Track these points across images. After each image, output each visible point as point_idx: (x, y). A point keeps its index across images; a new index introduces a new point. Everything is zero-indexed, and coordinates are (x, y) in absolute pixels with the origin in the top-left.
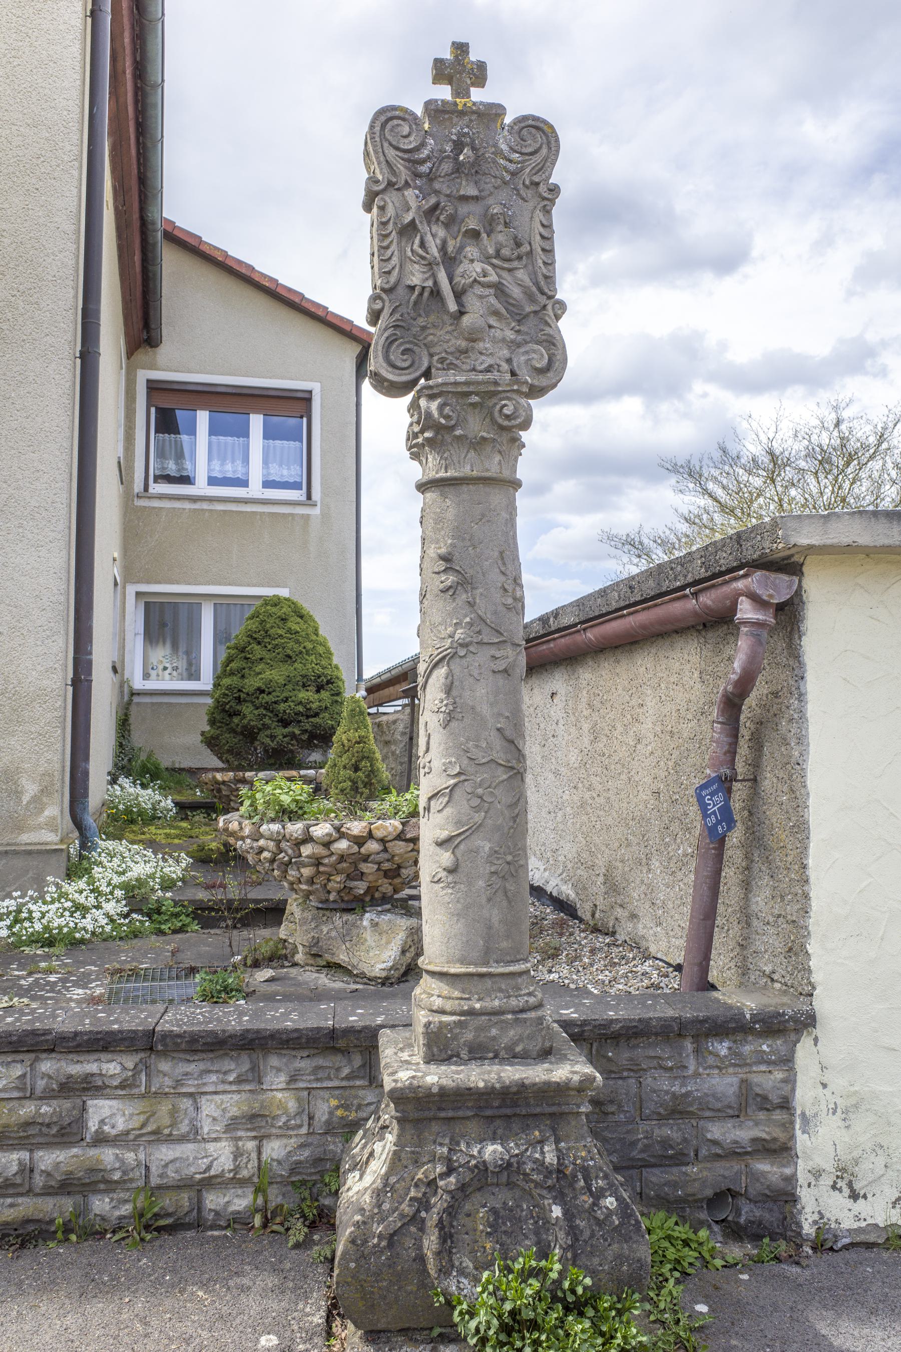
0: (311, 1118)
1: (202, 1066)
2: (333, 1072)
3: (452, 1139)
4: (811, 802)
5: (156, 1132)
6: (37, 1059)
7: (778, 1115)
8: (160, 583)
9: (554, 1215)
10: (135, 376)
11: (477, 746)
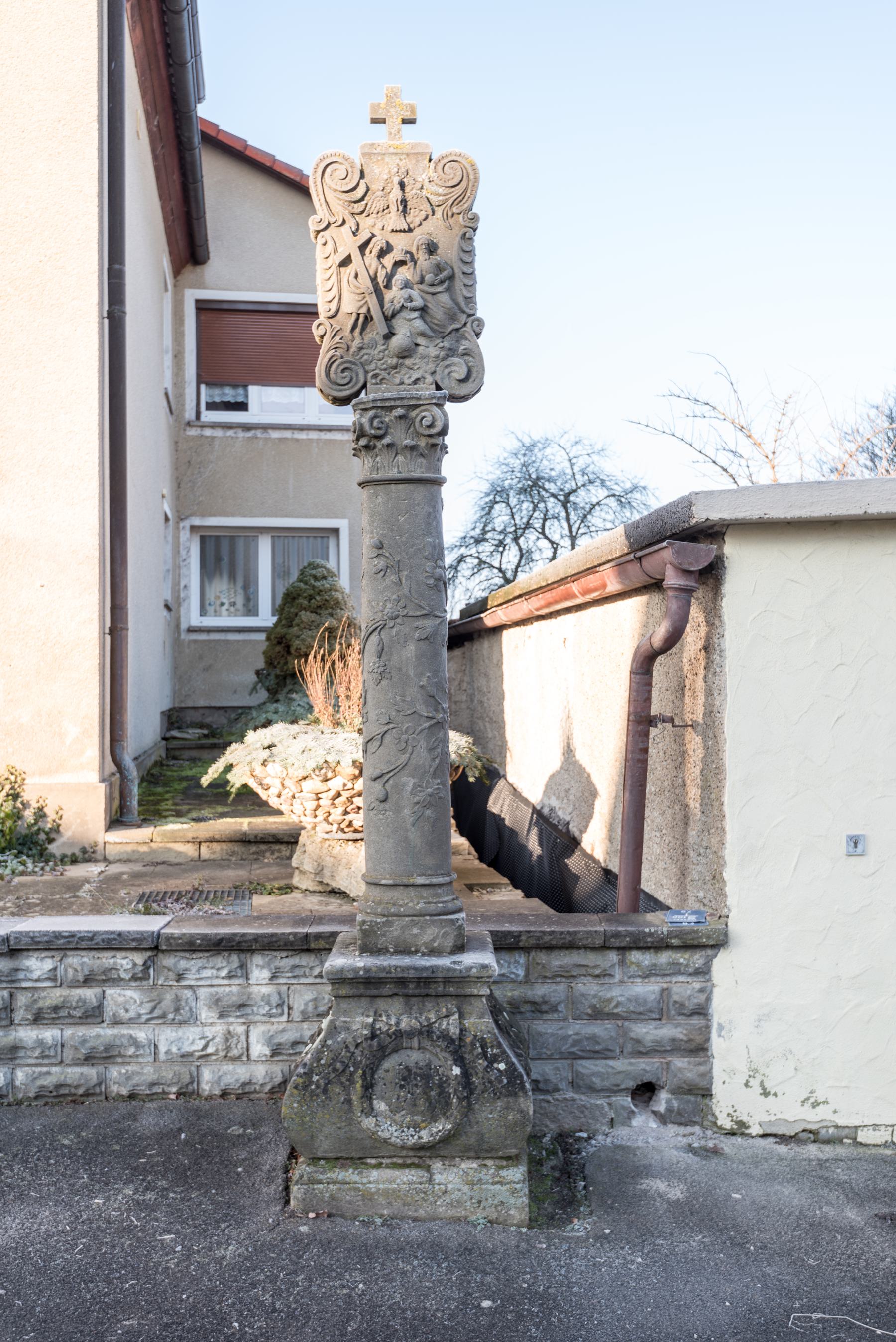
0: (290, 1008)
1: (200, 963)
2: (307, 970)
3: (375, 1013)
4: (727, 747)
5: (163, 1016)
6: (65, 956)
7: (696, 1021)
8: (214, 515)
9: (454, 1073)
10: (183, 296)
11: (403, 701)
